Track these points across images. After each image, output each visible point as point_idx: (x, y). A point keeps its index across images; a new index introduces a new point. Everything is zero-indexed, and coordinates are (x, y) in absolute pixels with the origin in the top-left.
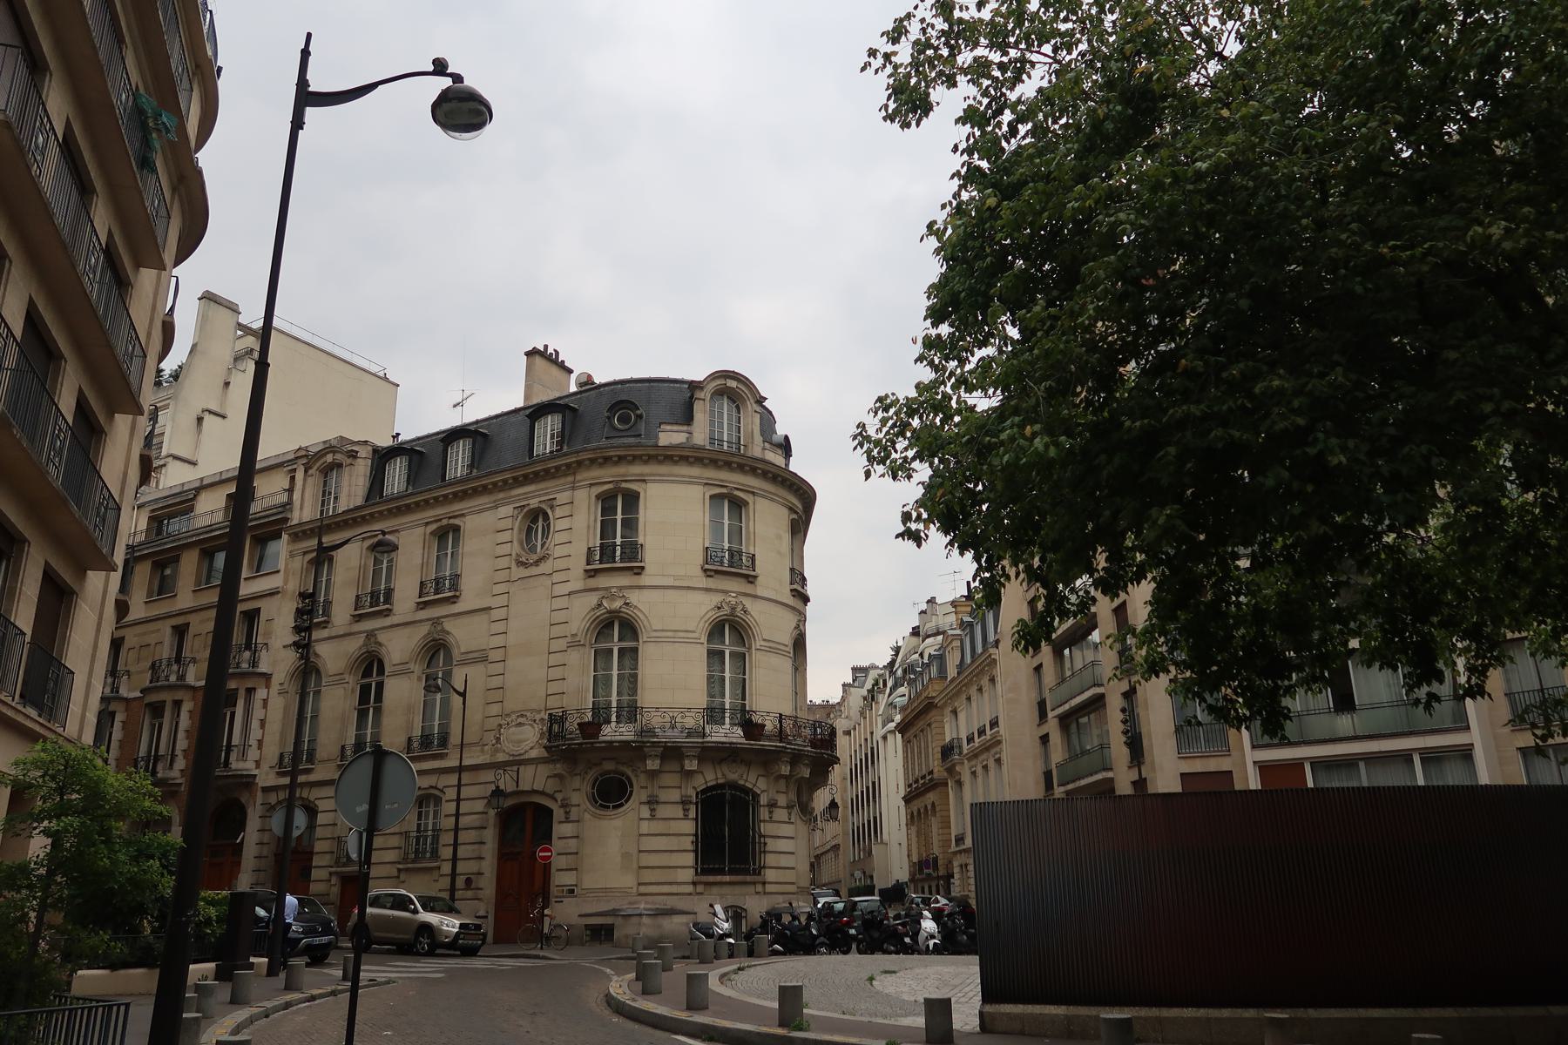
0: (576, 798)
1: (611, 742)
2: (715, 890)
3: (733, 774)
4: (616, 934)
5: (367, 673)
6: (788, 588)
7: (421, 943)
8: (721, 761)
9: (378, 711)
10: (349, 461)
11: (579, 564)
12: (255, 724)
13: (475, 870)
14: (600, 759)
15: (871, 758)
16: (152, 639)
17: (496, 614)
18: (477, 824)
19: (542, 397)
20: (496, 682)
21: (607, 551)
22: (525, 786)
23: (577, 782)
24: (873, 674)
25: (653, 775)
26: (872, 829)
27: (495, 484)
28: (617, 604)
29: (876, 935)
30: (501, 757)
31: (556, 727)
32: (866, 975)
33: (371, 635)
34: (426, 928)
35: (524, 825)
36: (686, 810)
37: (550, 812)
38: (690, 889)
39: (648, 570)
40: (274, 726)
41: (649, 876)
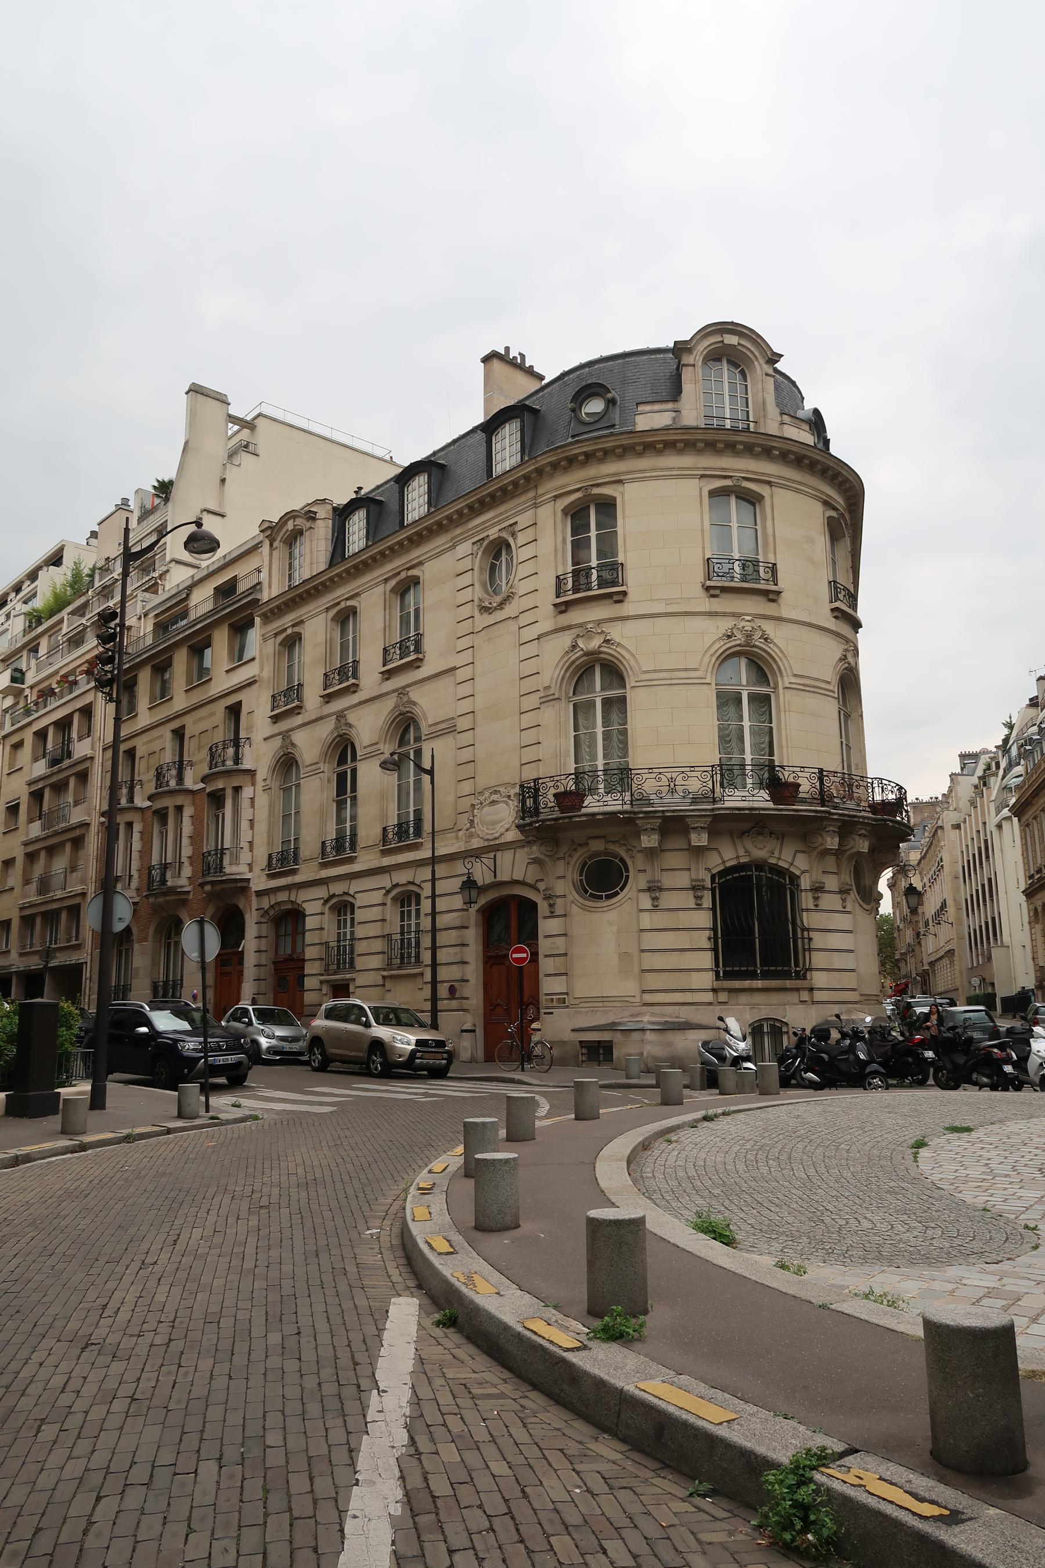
0: (560, 887)
1: (593, 815)
2: (744, 998)
3: (759, 850)
4: (616, 1053)
5: (342, 761)
6: (827, 607)
7: (376, 1063)
8: (742, 834)
9: (354, 799)
10: (308, 524)
11: (548, 597)
12: (244, 825)
13: (458, 976)
14: (588, 838)
15: (985, 852)
16: (156, 746)
17: (462, 674)
18: (457, 923)
19: (503, 402)
20: (466, 754)
21: (580, 574)
22: (504, 876)
23: (560, 868)
24: (984, 759)
25: (651, 854)
26: (990, 932)
27: (449, 518)
28: (595, 643)
29: (961, 1059)
30: (476, 843)
31: (529, 802)
32: (913, 1135)
33: (340, 716)
34: (377, 1044)
35: (508, 920)
36: (698, 898)
37: (533, 906)
38: (709, 997)
39: (631, 596)
40: (261, 827)
41: (654, 981)
